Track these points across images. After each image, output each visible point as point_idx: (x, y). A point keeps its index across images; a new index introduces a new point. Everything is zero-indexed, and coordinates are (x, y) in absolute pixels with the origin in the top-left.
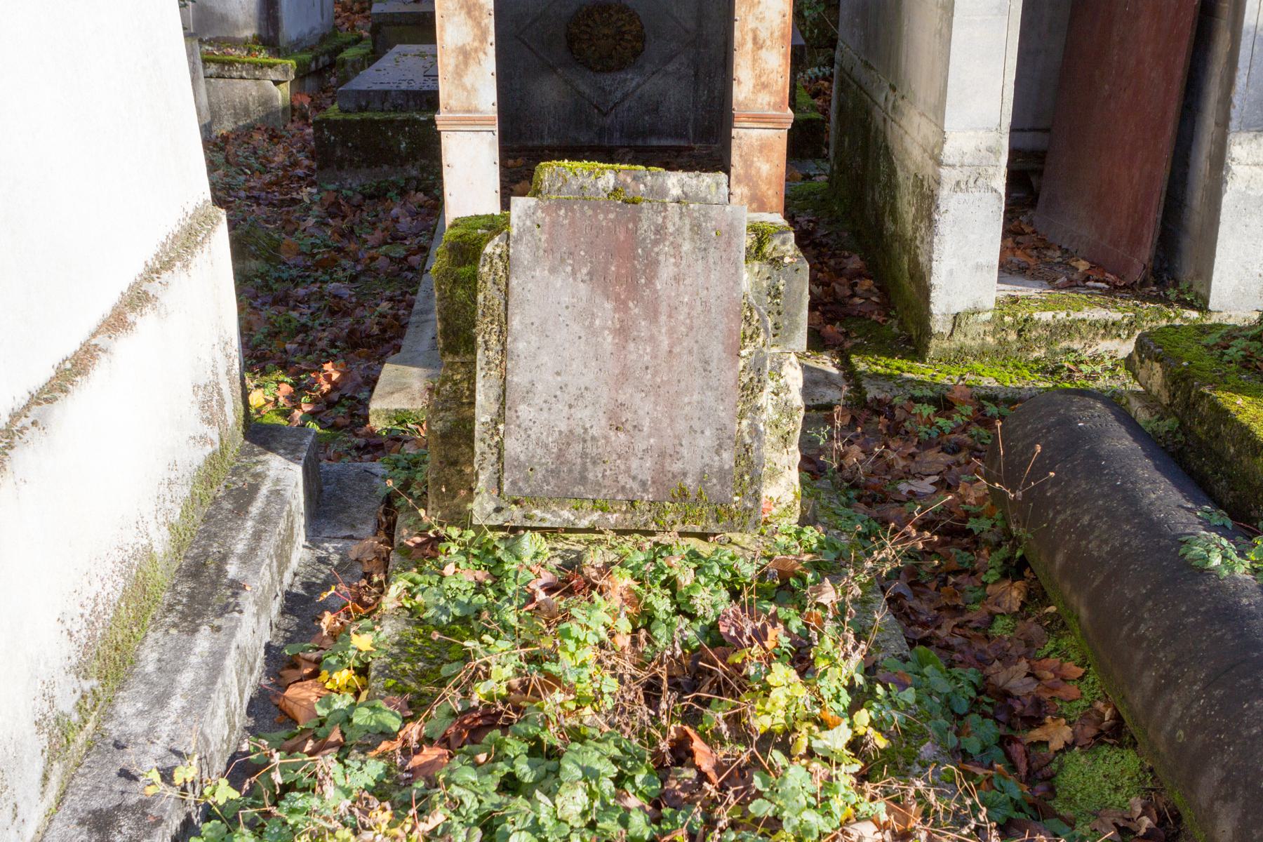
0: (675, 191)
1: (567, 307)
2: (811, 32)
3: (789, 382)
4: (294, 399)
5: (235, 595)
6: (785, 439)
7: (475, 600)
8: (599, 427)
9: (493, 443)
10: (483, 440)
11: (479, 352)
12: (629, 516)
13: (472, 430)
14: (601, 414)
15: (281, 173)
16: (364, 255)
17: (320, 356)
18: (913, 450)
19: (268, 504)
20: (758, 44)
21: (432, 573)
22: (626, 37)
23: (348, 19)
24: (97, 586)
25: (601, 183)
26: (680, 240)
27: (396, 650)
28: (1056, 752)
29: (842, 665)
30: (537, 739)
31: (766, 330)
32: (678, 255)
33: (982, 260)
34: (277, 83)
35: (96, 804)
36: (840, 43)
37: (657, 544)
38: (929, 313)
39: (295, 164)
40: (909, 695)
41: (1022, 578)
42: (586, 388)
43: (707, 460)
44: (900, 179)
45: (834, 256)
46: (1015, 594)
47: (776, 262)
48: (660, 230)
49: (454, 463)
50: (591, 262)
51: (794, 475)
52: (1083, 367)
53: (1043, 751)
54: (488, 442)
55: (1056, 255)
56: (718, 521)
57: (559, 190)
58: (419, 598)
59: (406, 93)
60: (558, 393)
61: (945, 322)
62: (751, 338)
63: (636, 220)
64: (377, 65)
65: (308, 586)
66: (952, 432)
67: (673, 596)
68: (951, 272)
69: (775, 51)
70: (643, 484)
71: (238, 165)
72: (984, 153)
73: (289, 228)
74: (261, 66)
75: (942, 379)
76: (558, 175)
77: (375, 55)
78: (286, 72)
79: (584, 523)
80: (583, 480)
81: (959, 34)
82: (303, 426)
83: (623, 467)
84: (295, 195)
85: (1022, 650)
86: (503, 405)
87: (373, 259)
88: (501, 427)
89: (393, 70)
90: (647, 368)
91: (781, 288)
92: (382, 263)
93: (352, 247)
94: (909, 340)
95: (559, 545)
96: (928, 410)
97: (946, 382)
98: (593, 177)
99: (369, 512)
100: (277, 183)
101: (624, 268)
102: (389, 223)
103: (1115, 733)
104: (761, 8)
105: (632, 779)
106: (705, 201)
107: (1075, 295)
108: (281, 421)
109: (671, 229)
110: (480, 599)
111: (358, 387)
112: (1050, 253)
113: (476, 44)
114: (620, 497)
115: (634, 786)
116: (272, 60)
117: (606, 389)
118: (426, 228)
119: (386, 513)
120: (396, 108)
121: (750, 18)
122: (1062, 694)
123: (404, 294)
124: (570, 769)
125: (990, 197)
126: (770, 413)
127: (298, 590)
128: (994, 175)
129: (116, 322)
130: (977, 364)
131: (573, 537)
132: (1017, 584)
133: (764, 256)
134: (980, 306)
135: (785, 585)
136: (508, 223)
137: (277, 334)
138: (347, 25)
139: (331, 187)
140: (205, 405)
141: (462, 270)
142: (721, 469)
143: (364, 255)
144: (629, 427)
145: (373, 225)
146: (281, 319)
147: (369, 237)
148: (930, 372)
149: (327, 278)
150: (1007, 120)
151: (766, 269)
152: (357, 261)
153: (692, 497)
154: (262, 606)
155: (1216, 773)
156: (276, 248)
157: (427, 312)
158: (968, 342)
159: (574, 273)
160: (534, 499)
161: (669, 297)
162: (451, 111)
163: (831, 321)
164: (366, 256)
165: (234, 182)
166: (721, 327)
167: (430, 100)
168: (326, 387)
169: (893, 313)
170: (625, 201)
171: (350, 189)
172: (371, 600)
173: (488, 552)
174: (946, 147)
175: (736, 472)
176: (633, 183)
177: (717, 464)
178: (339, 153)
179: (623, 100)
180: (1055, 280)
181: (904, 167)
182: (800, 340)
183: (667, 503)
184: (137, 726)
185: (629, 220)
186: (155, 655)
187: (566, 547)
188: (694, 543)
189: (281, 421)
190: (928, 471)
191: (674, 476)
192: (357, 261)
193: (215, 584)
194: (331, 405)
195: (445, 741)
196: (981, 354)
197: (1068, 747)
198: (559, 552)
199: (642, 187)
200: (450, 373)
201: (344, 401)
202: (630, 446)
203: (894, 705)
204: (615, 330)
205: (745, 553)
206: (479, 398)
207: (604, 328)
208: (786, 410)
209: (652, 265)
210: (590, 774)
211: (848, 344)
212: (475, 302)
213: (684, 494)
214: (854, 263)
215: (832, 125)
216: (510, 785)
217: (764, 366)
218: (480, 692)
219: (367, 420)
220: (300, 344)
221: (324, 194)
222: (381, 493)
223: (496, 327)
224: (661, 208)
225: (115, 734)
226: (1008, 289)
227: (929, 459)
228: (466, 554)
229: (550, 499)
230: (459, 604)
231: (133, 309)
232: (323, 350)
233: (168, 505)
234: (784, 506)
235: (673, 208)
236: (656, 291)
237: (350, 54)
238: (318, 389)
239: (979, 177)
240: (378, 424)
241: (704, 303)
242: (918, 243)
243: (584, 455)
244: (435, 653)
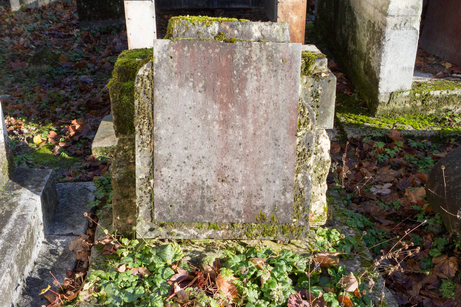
0: (257, 34)
1: (190, 108)
3: (323, 147)
4: (56, 139)
6: (319, 179)
8: (211, 180)
9: (147, 191)
10: (141, 189)
11: (137, 136)
12: (230, 232)
14: (212, 172)
15: (66, 22)
16: (99, 61)
17: (72, 115)
18: (375, 167)
19: (15, 226)
25: (210, 30)
26: (260, 65)
33: (406, 65)
38: (378, 92)
42: (203, 157)
43: (277, 198)
44: (359, 23)
47: (316, 76)
48: (247, 59)
50: (205, 80)
51: (324, 198)
54: (144, 190)
56: (283, 233)
57: (184, 34)
58: (102, 292)
60: (186, 160)
61: (385, 96)
62: (304, 124)
63: (232, 53)
65: (42, 272)
66: (395, 157)
67: (259, 289)
68: (390, 72)
70: (239, 213)
71: (47, 19)
72: (410, 9)
73: (66, 48)
75: (384, 126)
76: (183, 24)
80: (202, 211)
82: (59, 154)
83: (226, 204)
84: (71, 33)
86: (152, 168)
87: (103, 63)
88: (152, 181)
90: (240, 144)
91: (320, 92)
93: (93, 57)
94: (365, 105)
97: (387, 128)
98: (205, 26)
100: (64, 27)
101: (224, 82)
102: (111, 45)
106: (276, 40)
107: (448, 81)
108: (49, 152)
109: (254, 58)
110: (141, 290)
112: (430, 59)
114: (225, 221)
117: (215, 157)
127: (36, 275)
128: (415, 21)
130: (401, 118)
132: (452, 258)
133: (309, 72)
135: (324, 274)
136: (152, 56)
137: (53, 103)
139: (85, 29)
141: (126, 84)
142: (285, 203)
144: (229, 179)
146: (55, 96)
147: (102, 53)
148: (378, 122)
149: (81, 73)
151: (311, 81)
152: (96, 64)
153: (268, 220)
158: (397, 107)
159: (194, 87)
160: (173, 223)
161: (253, 101)
164: (100, 61)
165: (44, 27)
166: (285, 118)
168: (72, 133)
169: (355, 91)
170: (225, 41)
171: (95, 30)
174: (391, 6)
175: (294, 205)
176: (230, 30)
177: (283, 201)
178: (89, 13)
180: (436, 73)
181: (361, 17)
183: (253, 224)
185: (228, 53)
187: (193, 249)
189: (49, 152)
190: (385, 180)
191: (257, 208)
192: (96, 64)
194: (74, 142)
196: (403, 113)
198: (189, 253)
199: (236, 32)
200: (122, 145)
201: (81, 140)
202: (231, 191)
204: (221, 121)
207: (213, 120)
209: (243, 80)
212: (133, 104)
213: (263, 218)
217: (311, 141)
219: (91, 153)
220: (63, 109)
221: (83, 32)
223: (146, 121)
224: (248, 45)
227: (385, 173)
228: (132, 255)
229: (183, 223)
230: (127, 294)
232: (73, 112)
234: (318, 215)
235: (255, 45)
236: (246, 97)
238: (68, 134)
239: (407, 22)
240: (96, 154)
241: (275, 104)
242: (370, 56)
243: (203, 197)
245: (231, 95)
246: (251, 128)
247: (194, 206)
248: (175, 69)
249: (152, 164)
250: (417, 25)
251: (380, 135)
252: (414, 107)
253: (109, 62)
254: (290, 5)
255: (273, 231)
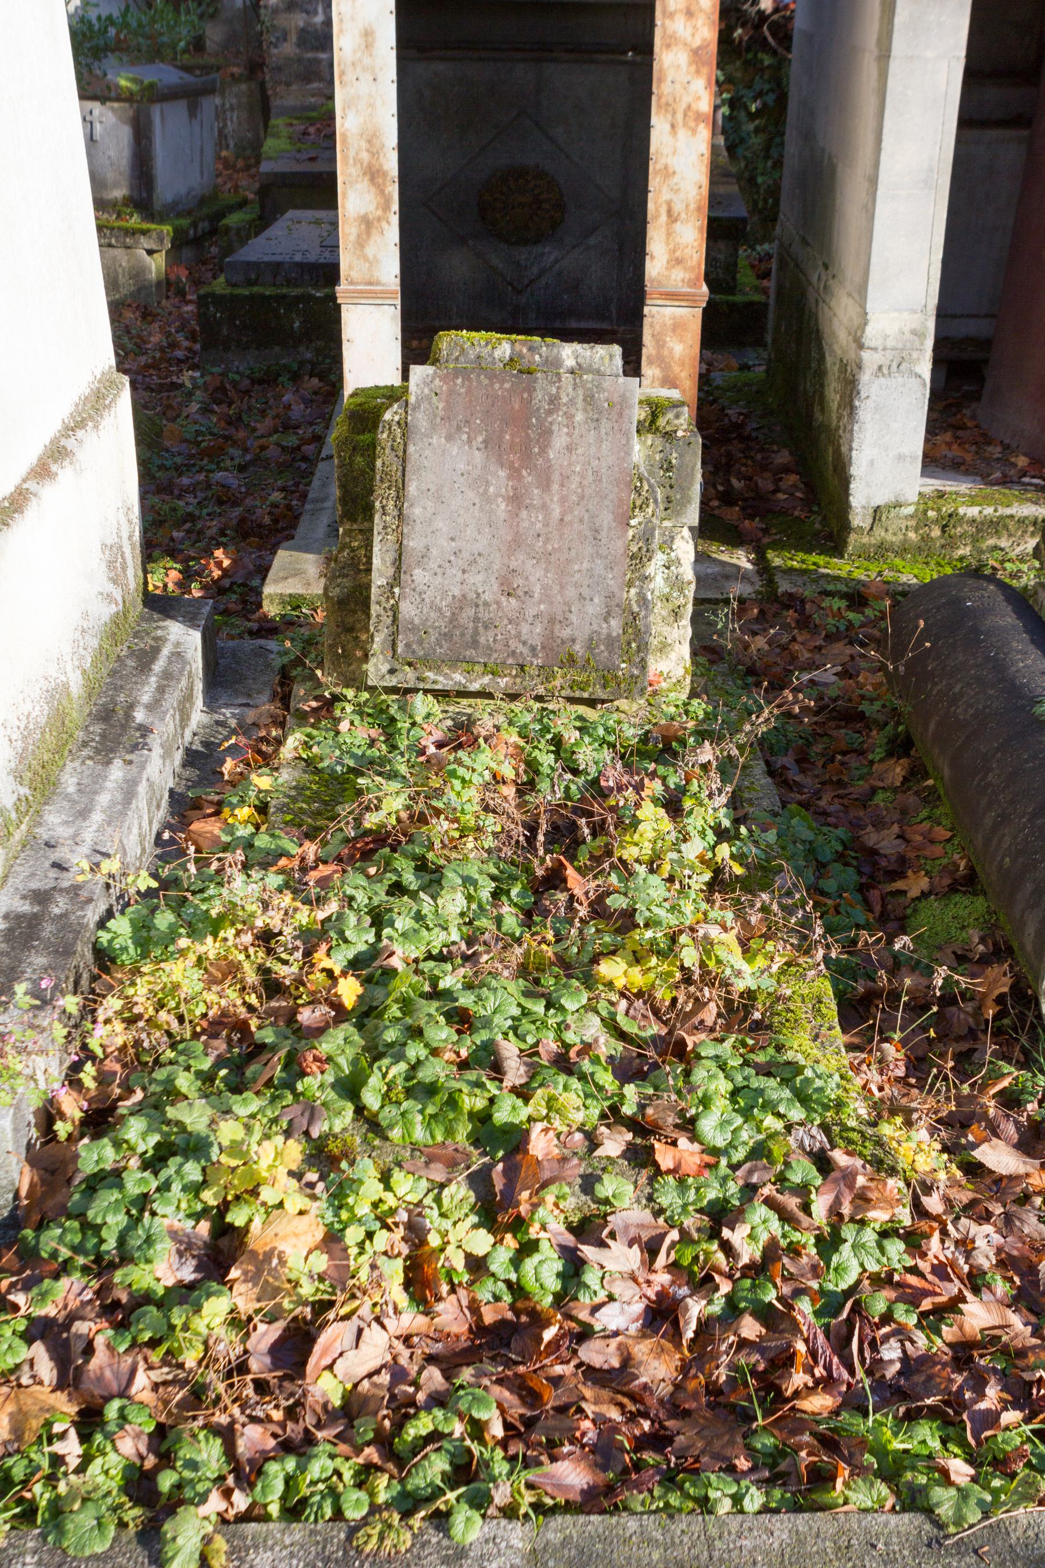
0: (570, 363)
2: (765, 201)
5: (143, 736)
7: (369, 752)
8: (490, 592)
10: (379, 603)
13: (368, 597)
15: (158, 355)
16: (253, 444)
20: (672, 217)
21: (327, 730)
22: (545, 206)
23: (230, 178)
24: (29, 706)
25: (497, 353)
27: (293, 793)
28: (913, 900)
29: (709, 809)
30: (423, 857)
31: (656, 501)
32: (570, 424)
33: (905, 450)
34: (150, 252)
35: (35, 885)
36: (781, 216)
37: (544, 709)
39: (173, 345)
40: (771, 836)
41: (908, 755)
43: (595, 627)
45: (762, 450)
46: (898, 770)
47: (669, 436)
48: (554, 400)
49: (350, 630)
51: (685, 650)
52: (1008, 565)
53: (901, 900)
55: (996, 451)
58: (315, 749)
59: (300, 265)
63: (531, 390)
64: (267, 233)
65: (206, 744)
68: (872, 463)
69: (690, 225)
70: (533, 649)
72: (908, 336)
74: (133, 232)
75: (859, 575)
77: (263, 222)
78: (161, 240)
79: (475, 687)
80: (475, 643)
81: (883, 209)
84: (175, 379)
85: (896, 816)
86: (398, 569)
87: (263, 448)
88: (397, 590)
89: (286, 238)
92: (273, 452)
93: (241, 434)
94: (830, 537)
95: (451, 709)
96: (838, 604)
99: (264, 684)
100: (154, 365)
101: (518, 436)
103: (968, 883)
104: (676, 179)
105: (508, 893)
106: (598, 372)
109: (565, 400)
111: (250, 575)
112: (990, 449)
113: (379, 213)
114: (510, 661)
115: (510, 899)
116: (145, 226)
117: (498, 555)
118: (322, 416)
119: (282, 684)
120: (289, 283)
121: (665, 189)
122: (927, 853)
123: (297, 484)
124: (451, 877)
125: (914, 382)
126: (659, 583)
127: (197, 746)
129: (42, 471)
130: (898, 561)
131: (465, 702)
134: (902, 499)
135: (668, 749)
138: (229, 185)
139: (216, 370)
140: (111, 565)
142: (609, 635)
143: (253, 444)
145: (263, 413)
146: (166, 507)
148: (848, 568)
150: (934, 301)
151: (659, 441)
153: (580, 662)
154: (166, 755)
155: (1029, 887)
156: (159, 434)
157: (323, 500)
158: (889, 537)
159: (470, 441)
160: (428, 662)
162: (351, 283)
163: (752, 517)
164: (256, 444)
167: (330, 273)
168: (217, 573)
169: (815, 508)
170: (520, 371)
172: (270, 749)
173: (382, 711)
174: (869, 329)
175: (624, 639)
178: (225, 332)
179: (540, 276)
181: (833, 351)
182: (692, 515)
184: (64, 832)
185: (524, 390)
186: (75, 780)
188: (582, 710)
191: (563, 642)
192: (246, 450)
193: (124, 727)
195: (339, 859)
196: (902, 550)
197: (925, 895)
203: (756, 843)
205: (629, 717)
206: (376, 562)
208: (677, 583)
209: (546, 433)
210: (468, 881)
211: (766, 540)
212: (373, 469)
213: (572, 660)
214: (783, 457)
215: (772, 308)
216: (397, 889)
217: (653, 535)
218: (371, 821)
219: (260, 606)
220: (188, 532)
221: (208, 378)
222: (278, 662)
225: (45, 837)
226: (934, 484)
228: (361, 713)
230: (354, 756)
231: (55, 461)
233: (82, 651)
235: (567, 379)
236: (549, 460)
237: (233, 220)
239: (901, 362)
240: (271, 609)
241: (595, 472)
243: (476, 619)
244: (331, 791)
245: (527, 457)
246: (556, 511)
247: (463, 635)
248: (441, 413)
249: (398, 563)
250: (925, 368)
251: (844, 589)
252: (926, 539)
253: (278, 444)
254: (669, 322)
255: (587, 683)
